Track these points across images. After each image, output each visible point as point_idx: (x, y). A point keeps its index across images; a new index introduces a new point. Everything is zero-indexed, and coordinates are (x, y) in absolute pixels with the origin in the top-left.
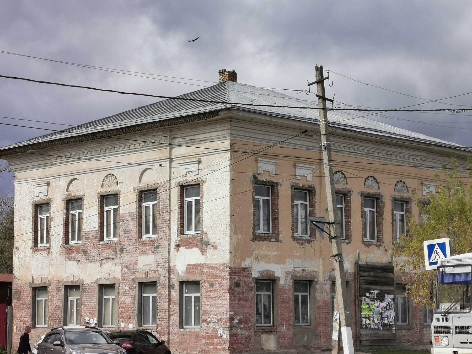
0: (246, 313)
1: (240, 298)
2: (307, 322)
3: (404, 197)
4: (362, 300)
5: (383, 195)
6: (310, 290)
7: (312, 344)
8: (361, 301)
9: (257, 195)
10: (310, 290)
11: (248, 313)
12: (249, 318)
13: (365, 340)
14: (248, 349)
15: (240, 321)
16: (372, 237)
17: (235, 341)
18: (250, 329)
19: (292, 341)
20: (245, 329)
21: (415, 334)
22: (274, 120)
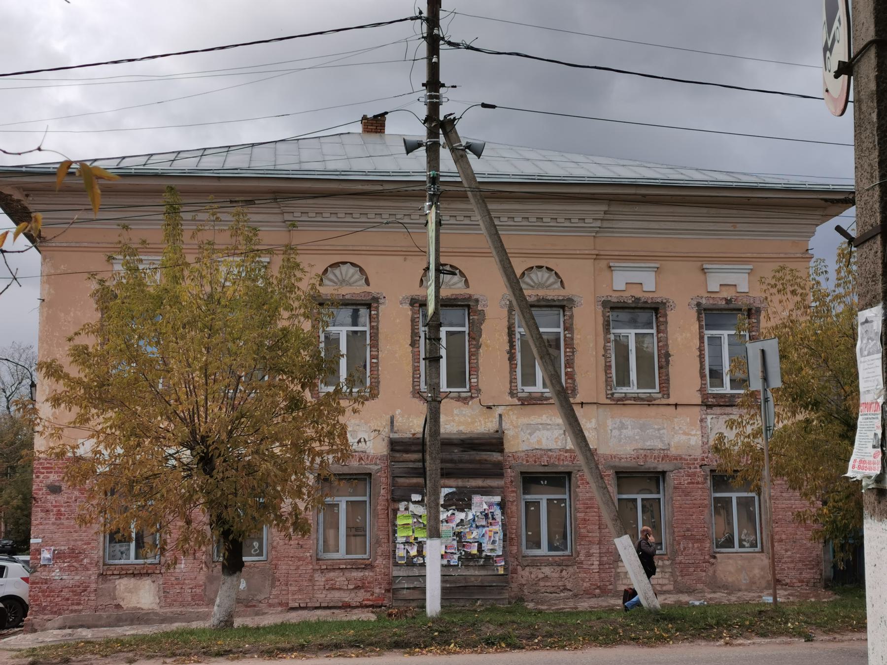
0: (76, 540)
1: (59, 514)
2: (260, 554)
3: (550, 298)
4: (398, 509)
5: (480, 298)
6: (570, 491)
7: (261, 597)
8: (396, 511)
9: (709, 327)
10: (570, 491)
11: (82, 540)
12: (84, 550)
13: (407, 588)
14: (81, 607)
15: (58, 556)
16: (645, 380)
17: (43, 591)
18: (86, 569)
19: (205, 590)
20: (71, 569)
21: (582, 575)
22: (223, 184)
